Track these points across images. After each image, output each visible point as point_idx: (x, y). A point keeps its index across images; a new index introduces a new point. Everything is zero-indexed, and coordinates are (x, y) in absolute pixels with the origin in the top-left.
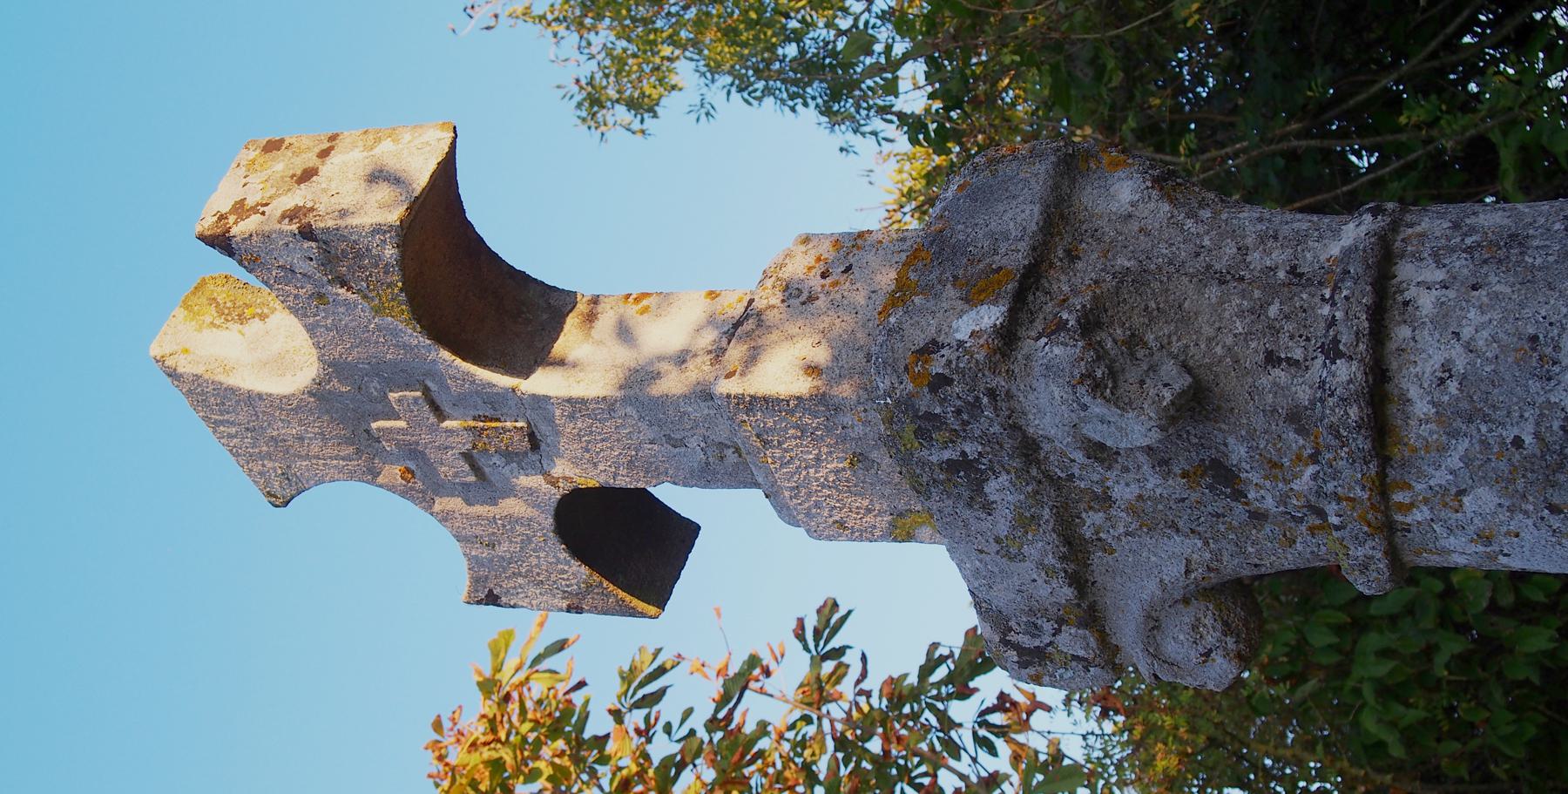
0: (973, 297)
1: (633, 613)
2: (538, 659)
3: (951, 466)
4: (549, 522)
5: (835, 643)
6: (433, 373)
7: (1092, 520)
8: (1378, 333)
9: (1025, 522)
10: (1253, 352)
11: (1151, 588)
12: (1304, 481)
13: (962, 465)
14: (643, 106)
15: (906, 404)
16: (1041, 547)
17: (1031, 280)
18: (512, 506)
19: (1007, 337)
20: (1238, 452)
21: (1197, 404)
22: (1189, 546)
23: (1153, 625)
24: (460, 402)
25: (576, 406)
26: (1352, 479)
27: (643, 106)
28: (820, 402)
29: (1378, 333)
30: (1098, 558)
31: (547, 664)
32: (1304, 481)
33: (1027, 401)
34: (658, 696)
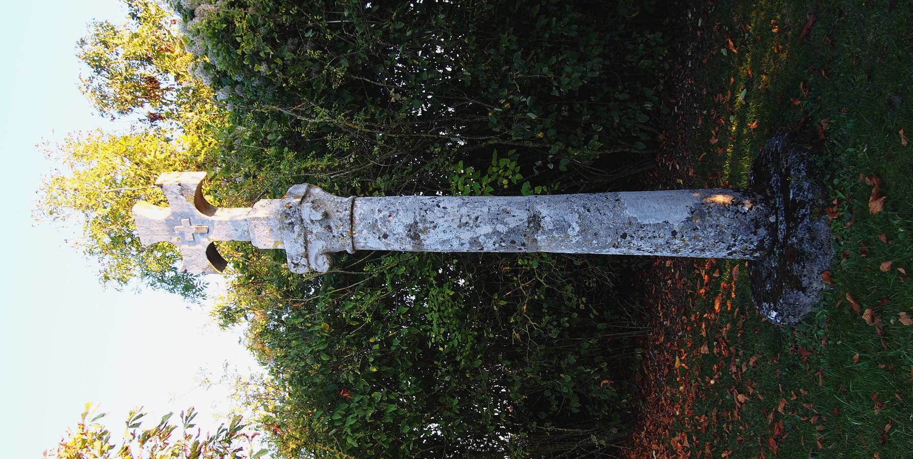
0: (295, 198)
1: (216, 273)
2: (94, 420)
3: (290, 224)
4: (205, 250)
5: (191, 423)
6: (193, 216)
7: (309, 236)
8: (352, 208)
9: (299, 235)
10: (335, 210)
11: (316, 251)
12: (341, 230)
13: (291, 223)
14: (123, 280)
15: (285, 212)
16: (301, 241)
17: (304, 198)
18: (199, 246)
19: (301, 203)
20: (332, 224)
21: (326, 215)
22: (323, 243)
23: (316, 259)
24: (196, 222)
25: (220, 222)
26: (348, 228)
27: (123, 280)
28: (268, 219)
29: (352, 208)
30: (309, 245)
31: (97, 421)
32: (341, 230)
33: (303, 212)
34: (138, 425)
